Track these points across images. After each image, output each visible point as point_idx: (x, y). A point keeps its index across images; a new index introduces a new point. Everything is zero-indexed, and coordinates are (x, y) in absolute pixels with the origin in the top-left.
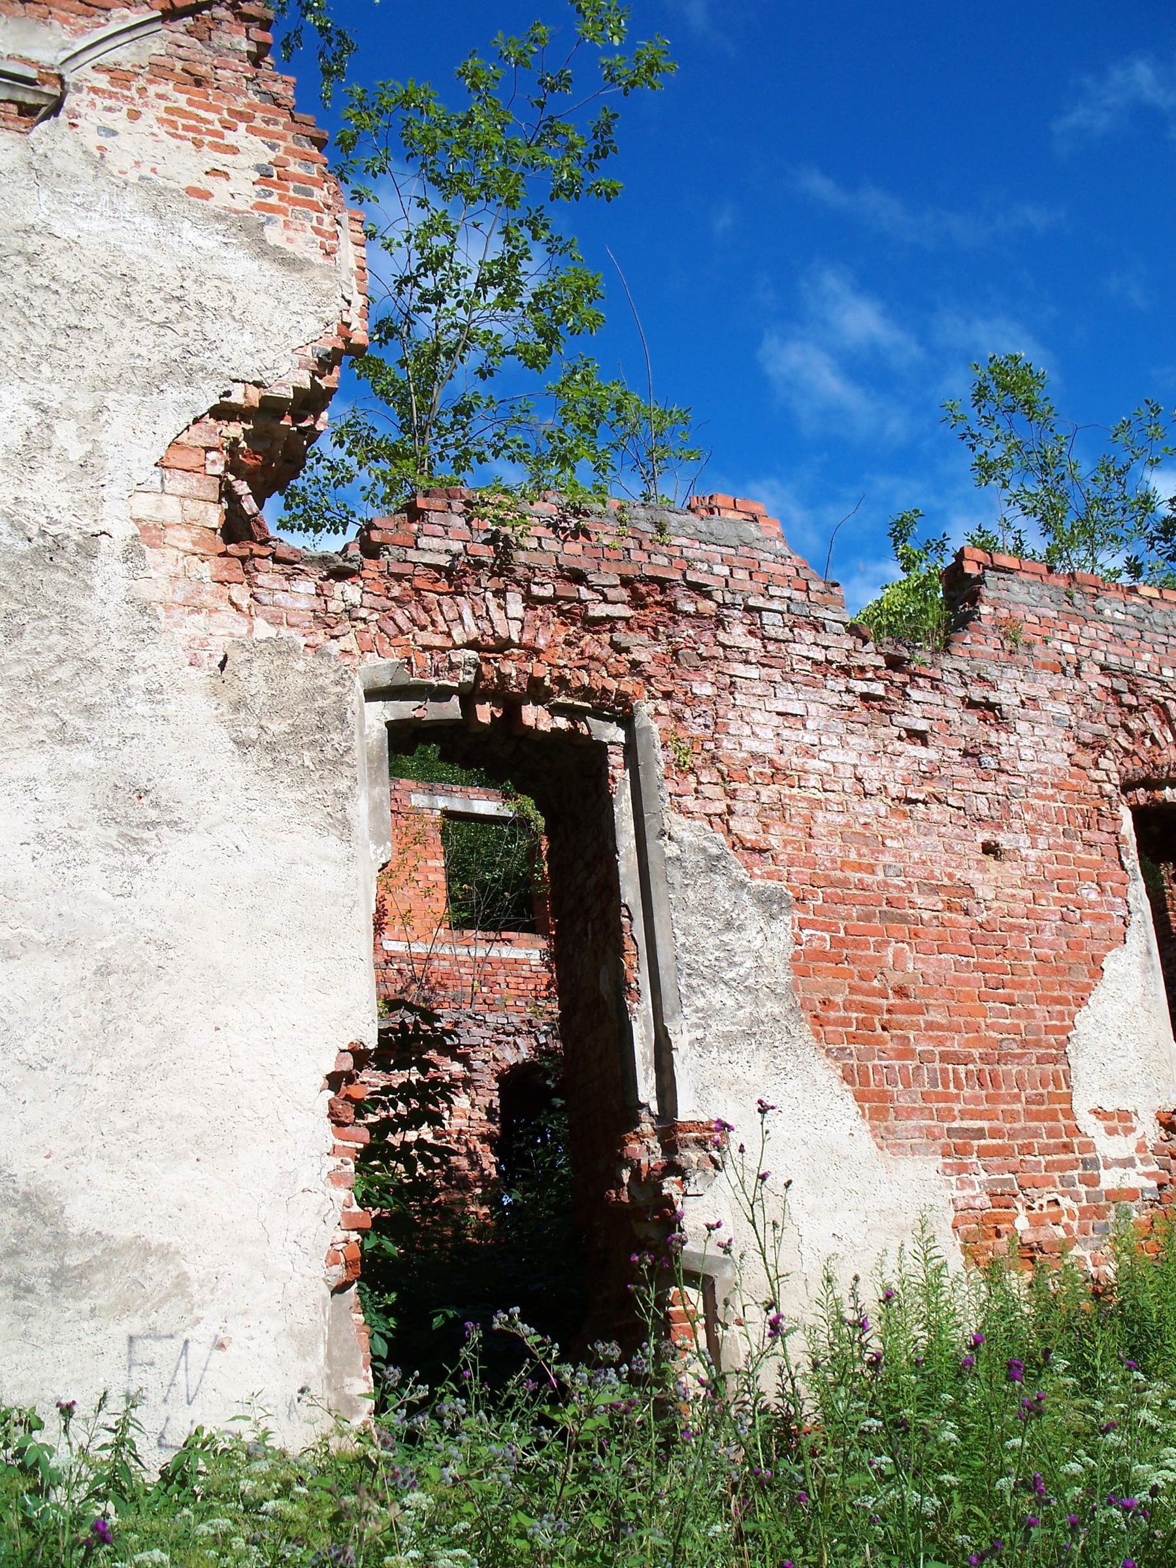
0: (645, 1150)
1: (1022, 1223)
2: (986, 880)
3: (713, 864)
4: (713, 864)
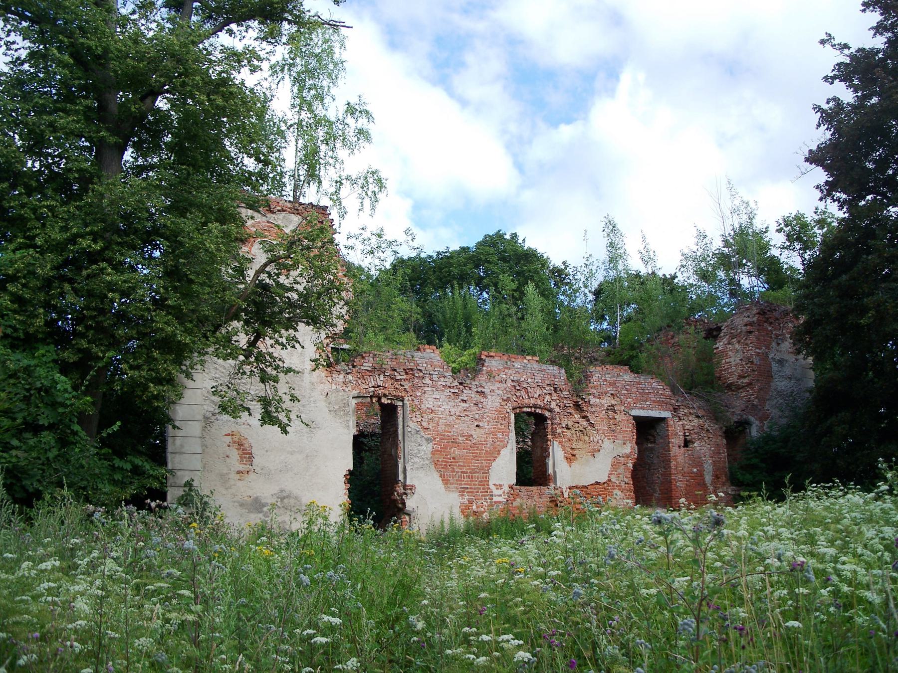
0: (400, 490)
1: (474, 507)
2: (476, 434)
3: (417, 432)
4: (417, 432)
